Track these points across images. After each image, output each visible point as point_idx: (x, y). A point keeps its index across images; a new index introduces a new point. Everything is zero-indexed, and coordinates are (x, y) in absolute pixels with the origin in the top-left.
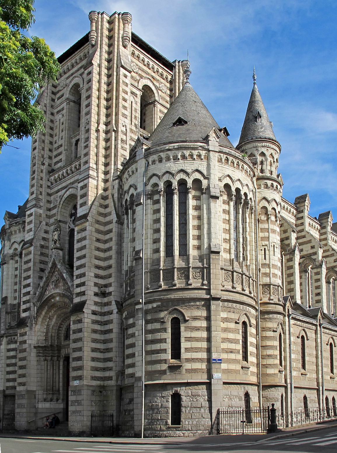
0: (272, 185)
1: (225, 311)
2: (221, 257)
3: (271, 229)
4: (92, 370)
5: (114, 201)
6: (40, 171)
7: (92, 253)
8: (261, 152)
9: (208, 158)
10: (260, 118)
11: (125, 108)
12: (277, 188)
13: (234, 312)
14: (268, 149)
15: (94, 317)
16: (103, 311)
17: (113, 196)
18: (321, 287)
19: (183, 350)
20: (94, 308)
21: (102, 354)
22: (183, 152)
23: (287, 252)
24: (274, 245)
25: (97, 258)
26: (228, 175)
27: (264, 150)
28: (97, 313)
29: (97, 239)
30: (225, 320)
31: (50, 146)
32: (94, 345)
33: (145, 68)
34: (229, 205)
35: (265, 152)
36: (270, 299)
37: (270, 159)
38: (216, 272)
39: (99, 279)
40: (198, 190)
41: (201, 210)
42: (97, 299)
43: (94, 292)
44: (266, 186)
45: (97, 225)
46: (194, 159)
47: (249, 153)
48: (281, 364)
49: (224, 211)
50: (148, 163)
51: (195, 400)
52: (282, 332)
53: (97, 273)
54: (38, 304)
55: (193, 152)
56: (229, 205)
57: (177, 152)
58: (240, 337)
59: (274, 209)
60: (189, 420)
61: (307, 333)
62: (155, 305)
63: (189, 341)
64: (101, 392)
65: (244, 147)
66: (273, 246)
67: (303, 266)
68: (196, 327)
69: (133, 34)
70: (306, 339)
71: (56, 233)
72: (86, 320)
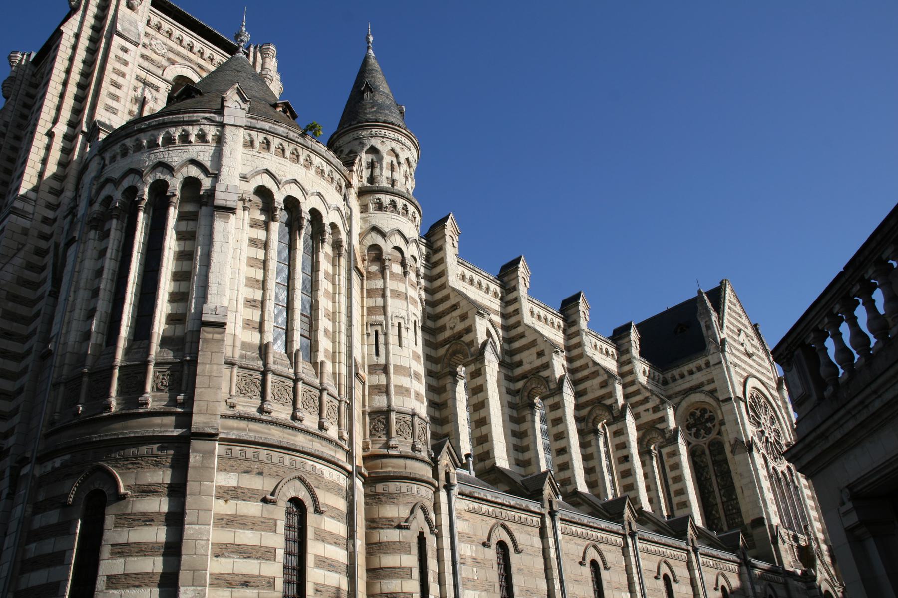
0: (394, 204)
1: (232, 469)
2: (228, 340)
9: (220, 140)
11: (116, 98)
12: (407, 211)
13: (261, 474)
14: (384, 139)
18: (565, 435)
22: (168, 132)
23: (470, 359)
24: (399, 324)
27: (376, 142)
30: (227, 494)
35: (379, 146)
36: (261, 410)
37: (387, 159)
38: (211, 372)
44: (380, 207)
45: (11, 304)
46: (190, 142)
47: (346, 151)
49: (253, 242)
52: (426, 530)
56: (267, 229)
57: (155, 132)
58: (277, 541)
61: (604, 553)
62: (58, 463)
63: (121, 554)
67: (526, 394)
68: (144, 514)
70: (310, 509)
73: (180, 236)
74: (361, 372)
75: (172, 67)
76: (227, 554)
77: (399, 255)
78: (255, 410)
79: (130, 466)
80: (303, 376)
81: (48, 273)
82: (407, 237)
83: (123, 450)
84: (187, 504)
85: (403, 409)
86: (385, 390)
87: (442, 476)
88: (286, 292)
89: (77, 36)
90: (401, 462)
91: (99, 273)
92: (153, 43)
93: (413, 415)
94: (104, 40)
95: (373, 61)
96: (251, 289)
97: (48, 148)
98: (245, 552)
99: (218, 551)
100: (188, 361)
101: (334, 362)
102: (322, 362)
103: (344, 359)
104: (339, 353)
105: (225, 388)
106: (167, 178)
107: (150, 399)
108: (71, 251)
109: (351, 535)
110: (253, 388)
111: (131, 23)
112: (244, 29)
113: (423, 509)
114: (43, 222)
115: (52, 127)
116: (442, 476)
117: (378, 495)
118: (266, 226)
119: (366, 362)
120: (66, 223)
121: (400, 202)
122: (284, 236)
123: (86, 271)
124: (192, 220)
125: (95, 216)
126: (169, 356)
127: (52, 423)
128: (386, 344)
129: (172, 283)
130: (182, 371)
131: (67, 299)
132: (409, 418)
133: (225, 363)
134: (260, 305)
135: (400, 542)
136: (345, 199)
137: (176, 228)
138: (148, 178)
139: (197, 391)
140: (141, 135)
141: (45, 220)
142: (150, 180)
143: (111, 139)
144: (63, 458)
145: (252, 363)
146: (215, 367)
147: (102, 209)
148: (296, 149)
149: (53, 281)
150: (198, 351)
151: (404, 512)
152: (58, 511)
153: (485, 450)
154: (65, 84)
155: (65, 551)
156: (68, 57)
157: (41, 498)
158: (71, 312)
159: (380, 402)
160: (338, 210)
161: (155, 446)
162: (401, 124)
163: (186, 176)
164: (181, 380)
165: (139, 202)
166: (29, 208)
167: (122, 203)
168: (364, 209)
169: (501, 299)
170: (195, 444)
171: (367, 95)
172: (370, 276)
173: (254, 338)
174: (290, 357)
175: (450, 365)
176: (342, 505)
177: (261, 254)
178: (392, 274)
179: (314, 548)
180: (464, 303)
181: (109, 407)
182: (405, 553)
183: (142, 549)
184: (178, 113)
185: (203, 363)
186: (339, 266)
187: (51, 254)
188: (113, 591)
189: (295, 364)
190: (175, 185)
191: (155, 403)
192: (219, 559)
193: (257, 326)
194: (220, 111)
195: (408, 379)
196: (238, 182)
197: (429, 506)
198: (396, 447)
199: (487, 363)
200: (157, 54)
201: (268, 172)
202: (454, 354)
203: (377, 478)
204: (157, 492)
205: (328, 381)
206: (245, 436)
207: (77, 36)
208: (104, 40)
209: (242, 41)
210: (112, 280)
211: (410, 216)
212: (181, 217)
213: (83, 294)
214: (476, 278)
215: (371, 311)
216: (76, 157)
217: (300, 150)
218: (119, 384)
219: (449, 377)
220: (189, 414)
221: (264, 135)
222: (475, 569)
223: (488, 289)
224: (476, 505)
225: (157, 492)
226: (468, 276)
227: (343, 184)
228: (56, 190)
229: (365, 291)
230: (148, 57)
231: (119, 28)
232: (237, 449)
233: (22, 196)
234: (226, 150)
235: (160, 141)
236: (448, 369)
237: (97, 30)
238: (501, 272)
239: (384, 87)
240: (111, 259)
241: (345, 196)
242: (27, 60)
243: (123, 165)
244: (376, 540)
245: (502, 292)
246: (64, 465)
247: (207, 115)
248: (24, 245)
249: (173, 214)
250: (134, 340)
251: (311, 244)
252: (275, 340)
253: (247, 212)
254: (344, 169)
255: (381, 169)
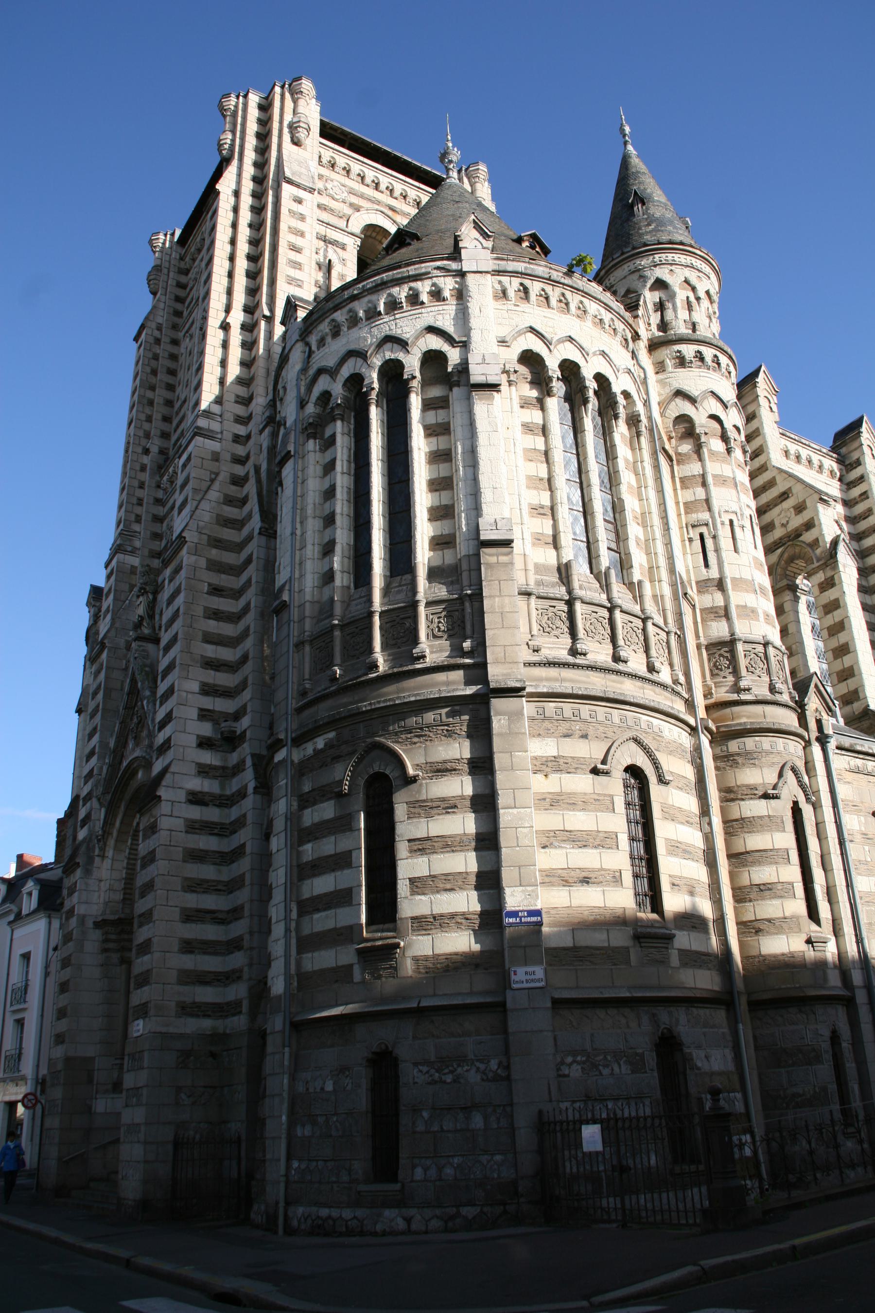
0: (700, 357)
1: (548, 733)
3: (714, 476)
4: (180, 982)
5: (259, 481)
6: (138, 468)
7: (195, 625)
8: (652, 281)
9: (461, 295)
10: (643, 204)
11: (297, 265)
12: (719, 364)
13: (585, 736)
14: (673, 268)
15: (195, 813)
16: (228, 792)
17: (257, 469)
19: (403, 888)
20: (196, 784)
21: (223, 927)
22: (390, 295)
23: (816, 564)
24: (731, 522)
25: (209, 639)
26: (531, 327)
27: (661, 273)
28: (207, 798)
29: (215, 589)
31: (165, 410)
32: (192, 900)
33: (370, 192)
34: (543, 408)
36: (574, 652)
37: (682, 295)
39: (217, 699)
40: (435, 384)
41: (450, 434)
42: (207, 757)
43: (198, 736)
44: (682, 362)
45: (214, 551)
46: (423, 303)
48: (813, 914)
49: (528, 428)
50: (310, 348)
51: (449, 1078)
52: (801, 799)
53: (211, 681)
54: (108, 797)
55: (418, 285)
56: (543, 408)
57: (373, 297)
59: (714, 417)
60: (429, 1162)
62: (320, 743)
63: (422, 851)
64: (213, 1055)
65: (607, 281)
66: (727, 523)
68: (443, 800)
69: (322, 123)
71: (141, 599)
72: (164, 823)
73: (431, 431)
74: (689, 591)
75: (358, 214)
76: (556, 844)
77: (717, 426)
78: (565, 652)
79: (416, 740)
80: (619, 602)
81: (253, 505)
82: (725, 400)
83: (404, 720)
84: (498, 782)
85: (751, 637)
86: (726, 614)
87: (812, 725)
88: (579, 491)
89: (237, 194)
90: (759, 709)
91: (330, 493)
92: (329, 186)
93: (766, 644)
94: (271, 192)
95: (636, 161)
96: (535, 492)
97: (225, 345)
98: (579, 840)
99: (544, 840)
100: (469, 596)
101: (652, 581)
102: (640, 583)
103: (664, 574)
104: (658, 567)
105: (524, 628)
106: (401, 356)
107: (428, 651)
108: (287, 472)
109: (705, 811)
110: (559, 623)
111: (300, 164)
112: (450, 145)
113: (794, 770)
114: (234, 441)
115: (226, 318)
116: (812, 725)
117: (732, 755)
118: (541, 404)
119: (693, 578)
120: (265, 439)
121: (708, 353)
122: (565, 415)
123: (311, 493)
124: (442, 408)
125: (311, 420)
126: (441, 592)
127: (304, 693)
128: (717, 550)
129: (429, 495)
130: (463, 610)
131: (293, 534)
132: (760, 648)
133: (519, 594)
134: (549, 512)
135: (769, 816)
136: (634, 355)
137: (422, 420)
138: (375, 360)
139: (489, 634)
140: (356, 305)
141: (237, 439)
142: (377, 361)
143: (315, 317)
144: (326, 736)
145: (551, 590)
146: (507, 600)
147: (318, 410)
148: (563, 295)
149: (261, 516)
150: (481, 581)
151: (772, 778)
152: (332, 802)
153: (852, 688)
154: (232, 258)
155: (350, 852)
156: (230, 222)
157: (307, 788)
158: (301, 549)
159: (719, 630)
160: (629, 372)
161: (444, 711)
162: (688, 240)
163: (425, 349)
164: (463, 622)
165: (367, 394)
166: (215, 426)
167: (345, 398)
168: (660, 367)
169: (840, 480)
170: (497, 703)
171: (638, 209)
172: (682, 459)
173: (550, 557)
174: (597, 577)
175: (786, 576)
176: (689, 772)
177: (539, 443)
178: (712, 453)
179: (663, 830)
180: (797, 489)
181: (374, 666)
182: (778, 831)
183: (447, 844)
184: (400, 267)
185: (490, 596)
186: (640, 449)
187: (252, 481)
188: (419, 897)
189: (606, 587)
190: (412, 363)
191: (435, 656)
192: (547, 850)
193: (550, 540)
194: (456, 254)
195: (753, 596)
196: (495, 348)
197: (800, 765)
198: (749, 690)
199: (841, 568)
200: (336, 200)
201: (532, 330)
202: (792, 559)
203: (727, 734)
204: (455, 770)
205: (651, 608)
206: (558, 688)
207: (237, 194)
208: (271, 192)
209: (451, 162)
210: (349, 501)
211: (724, 370)
212: (428, 405)
213: (313, 525)
214: (804, 453)
215: (689, 507)
216: (261, 351)
217: (568, 294)
218: (382, 636)
219: (788, 592)
220: (482, 666)
221: (519, 280)
222: (867, 848)
223: (821, 467)
224: (859, 762)
225: (455, 770)
226: (792, 452)
227: (629, 336)
228: (243, 398)
229: (677, 480)
230: (326, 210)
231: (288, 173)
232: (551, 707)
233: (204, 411)
234: (473, 306)
235: (381, 308)
236: (785, 582)
237: (259, 180)
238: (834, 442)
239: (657, 195)
240: (343, 473)
241: (633, 352)
242: (171, 241)
243: (334, 350)
244: (736, 815)
245: (840, 470)
246: (329, 745)
247: (439, 263)
248: (217, 474)
249: (415, 402)
250: (392, 576)
251: (600, 423)
252: (576, 556)
253: (513, 388)
254: (627, 315)
255: (675, 309)
